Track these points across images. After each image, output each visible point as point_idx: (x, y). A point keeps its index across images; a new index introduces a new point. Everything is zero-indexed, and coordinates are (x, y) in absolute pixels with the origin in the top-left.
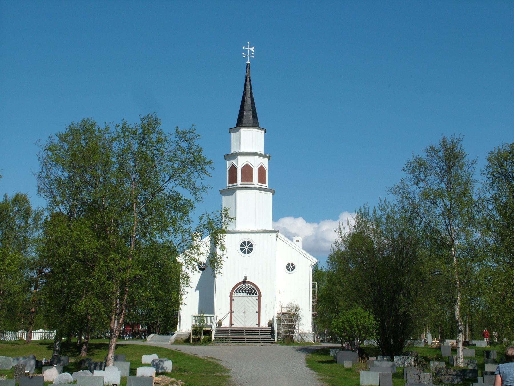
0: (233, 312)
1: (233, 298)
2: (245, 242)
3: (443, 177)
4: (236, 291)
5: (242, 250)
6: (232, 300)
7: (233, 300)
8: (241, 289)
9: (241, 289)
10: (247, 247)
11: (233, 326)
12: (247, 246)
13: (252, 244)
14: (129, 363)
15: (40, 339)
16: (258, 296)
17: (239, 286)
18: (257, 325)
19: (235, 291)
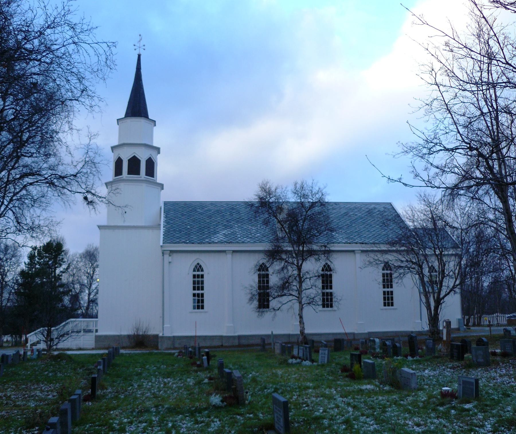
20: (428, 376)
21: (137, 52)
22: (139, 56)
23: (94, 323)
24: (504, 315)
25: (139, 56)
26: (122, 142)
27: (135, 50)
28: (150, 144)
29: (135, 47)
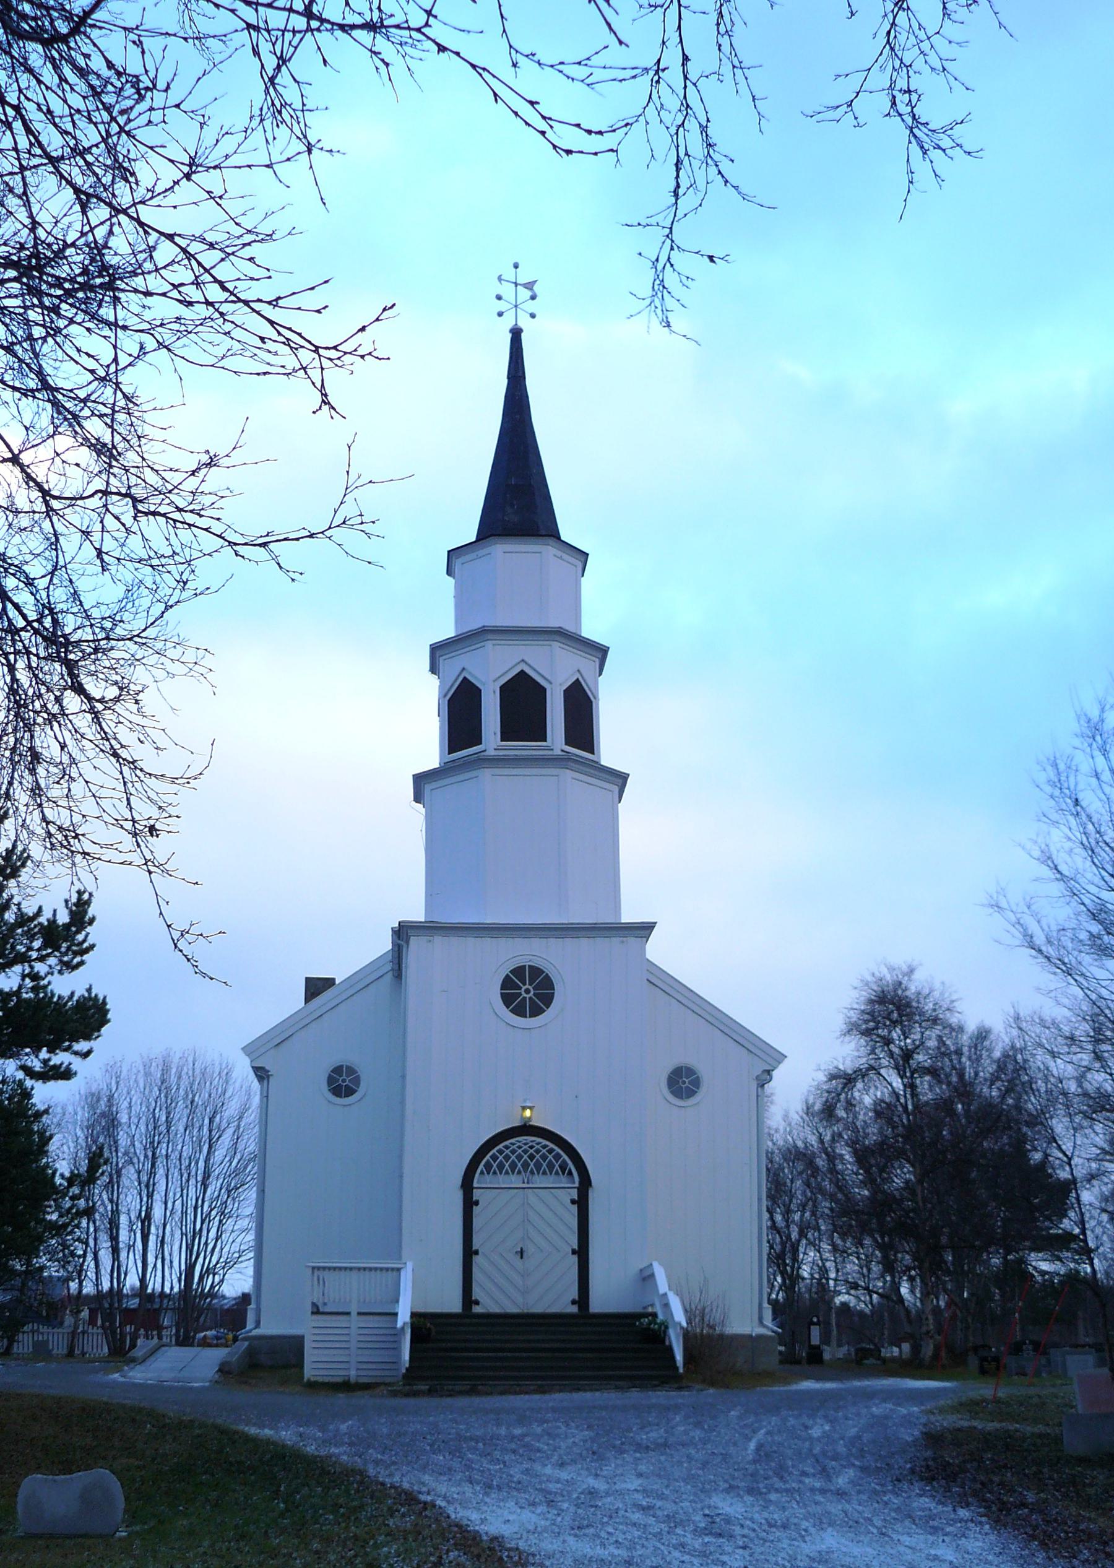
0: (477, 1253)
1: (477, 1194)
2: (519, 971)
3: (739, 1494)
4: (488, 1166)
5: (507, 1000)
6: (469, 1204)
7: (477, 1203)
8: (507, 1158)
9: (507, 1158)
10: (527, 991)
11: (477, 1309)
12: (527, 986)
13: (547, 977)
14: (310, 1371)
15: (106, 1285)
16: (577, 1185)
17: (500, 1146)
18: (573, 1302)
19: (481, 1166)
20: (952, 1048)
21: (508, 322)
22: (516, 334)
23: (61, 1337)
24: (50, 1330)
25: (516, 334)
26: (474, 625)
27: (500, 314)
28: (609, 919)
29: (501, 306)
